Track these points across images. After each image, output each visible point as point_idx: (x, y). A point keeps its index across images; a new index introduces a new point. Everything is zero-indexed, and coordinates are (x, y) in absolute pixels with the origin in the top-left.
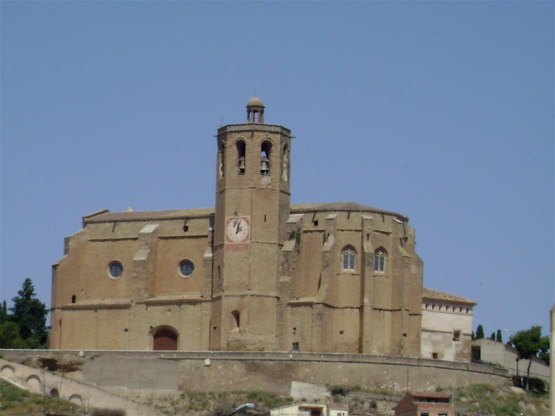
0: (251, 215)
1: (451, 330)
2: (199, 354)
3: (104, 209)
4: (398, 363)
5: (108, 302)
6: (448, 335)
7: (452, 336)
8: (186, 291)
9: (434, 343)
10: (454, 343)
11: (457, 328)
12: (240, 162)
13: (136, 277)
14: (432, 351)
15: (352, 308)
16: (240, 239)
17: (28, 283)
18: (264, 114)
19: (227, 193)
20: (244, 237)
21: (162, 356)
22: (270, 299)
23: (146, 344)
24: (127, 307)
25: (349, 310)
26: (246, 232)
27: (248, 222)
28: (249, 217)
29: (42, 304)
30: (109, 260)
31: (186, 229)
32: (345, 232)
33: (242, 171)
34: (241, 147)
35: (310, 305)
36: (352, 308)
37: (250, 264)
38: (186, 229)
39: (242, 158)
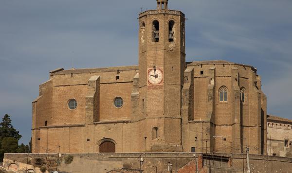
0: (164, 67)
1: (283, 139)
2: (135, 154)
3: (61, 68)
4: (260, 159)
5: (68, 124)
6: (282, 142)
7: (284, 143)
8: (119, 117)
9: (274, 148)
10: (285, 148)
11: (286, 139)
12: (155, 34)
13: (88, 108)
14: (272, 152)
15: (227, 125)
16: (157, 82)
17: (7, 116)
18: (168, 4)
19: (148, 54)
20: (159, 81)
21: (112, 156)
22: (177, 120)
23: (94, 149)
24: (83, 126)
25: (224, 127)
26: (161, 78)
27: (162, 72)
28: (162, 68)
29: (17, 131)
30: (68, 99)
31: (118, 78)
32: (221, 78)
33: (157, 40)
34: (156, 24)
35: (198, 122)
36: (227, 125)
37: (96, 119)
38: (118, 78)
39: (156, 32)
